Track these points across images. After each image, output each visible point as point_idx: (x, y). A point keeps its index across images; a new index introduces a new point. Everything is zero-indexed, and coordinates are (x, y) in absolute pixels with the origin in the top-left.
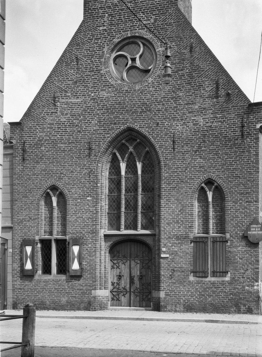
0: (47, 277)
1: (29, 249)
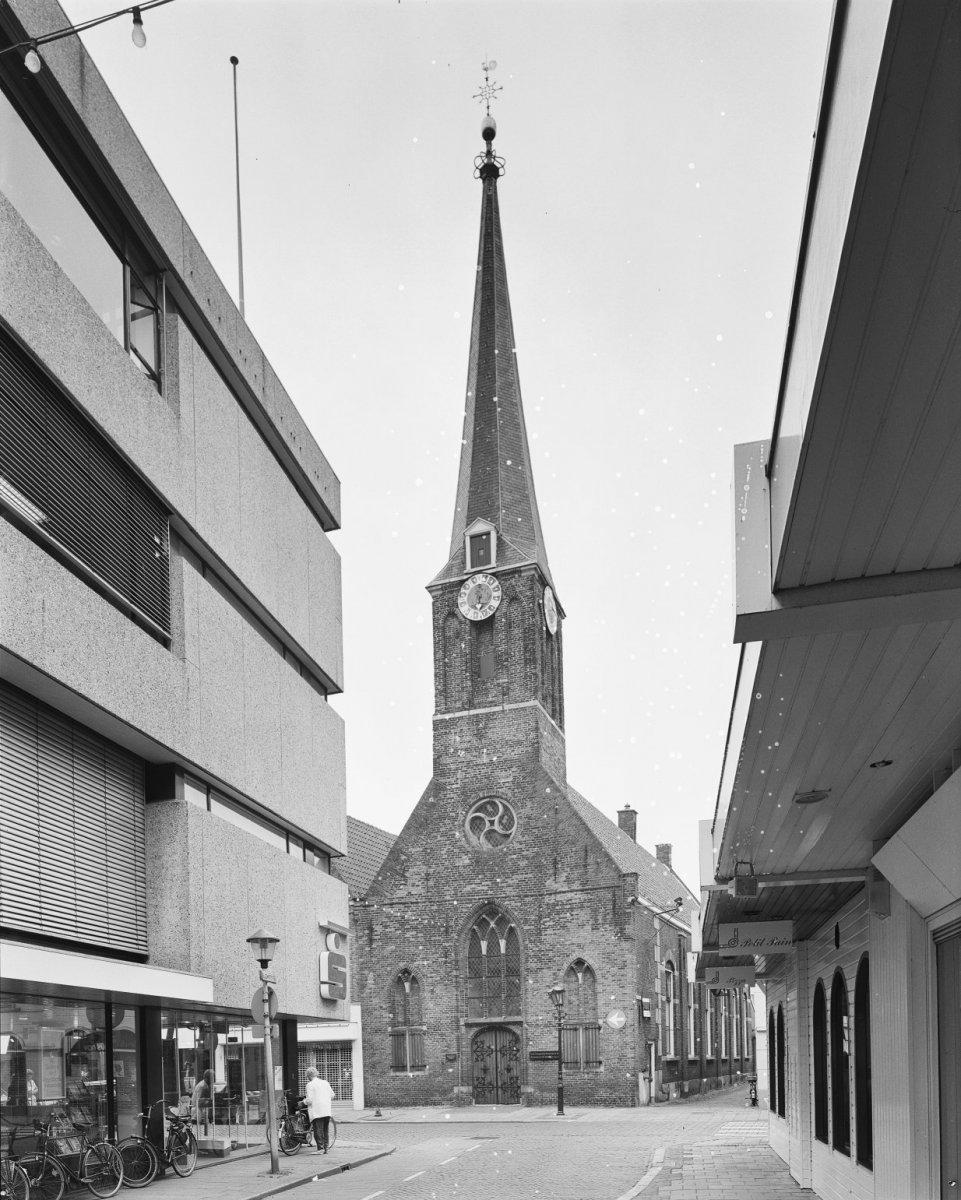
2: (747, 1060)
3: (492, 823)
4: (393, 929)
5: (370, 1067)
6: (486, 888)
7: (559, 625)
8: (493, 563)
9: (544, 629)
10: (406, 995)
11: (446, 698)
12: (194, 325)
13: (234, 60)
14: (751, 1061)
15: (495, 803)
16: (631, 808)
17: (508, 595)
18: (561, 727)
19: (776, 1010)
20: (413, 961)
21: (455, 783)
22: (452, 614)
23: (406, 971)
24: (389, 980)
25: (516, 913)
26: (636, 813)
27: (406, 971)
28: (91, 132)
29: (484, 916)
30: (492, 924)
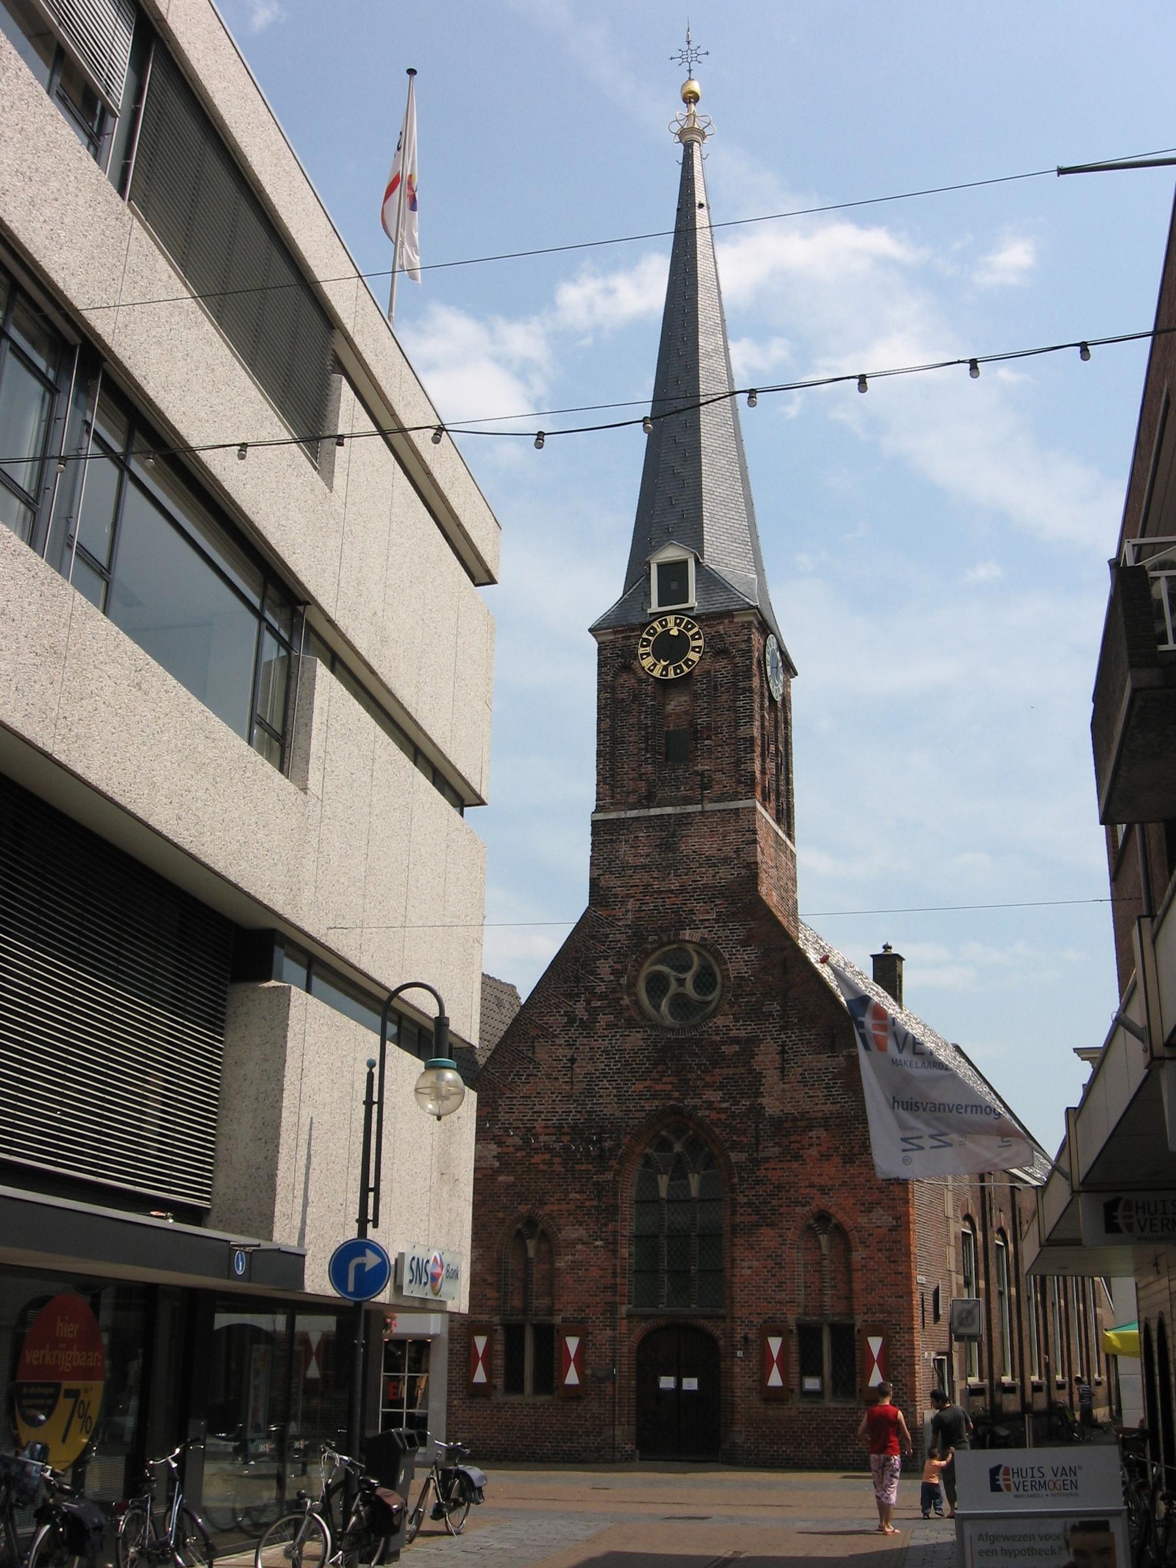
0: (515, 1399)
1: (480, 1342)
2: (1099, 1383)
3: (681, 982)
4: (512, 1149)
5: (465, 1391)
6: (669, 1087)
7: (786, 685)
8: (693, 601)
9: (767, 694)
10: (527, 1261)
11: (612, 787)
12: (412, 472)
13: (412, 72)
14: (1105, 1384)
15: (686, 951)
16: (893, 951)
17: (711, 647)
18: (790, 836)
19: (1154, 1325)
20: (542, 1203)
21: (627, 913)
22: (627, 668)
23: (531, 1222)
25: (717, 1131)
26: (902, 959)
27: (531, 1222)
28: (172, 26)
29: (663, 1133)
30: (678, 1148)
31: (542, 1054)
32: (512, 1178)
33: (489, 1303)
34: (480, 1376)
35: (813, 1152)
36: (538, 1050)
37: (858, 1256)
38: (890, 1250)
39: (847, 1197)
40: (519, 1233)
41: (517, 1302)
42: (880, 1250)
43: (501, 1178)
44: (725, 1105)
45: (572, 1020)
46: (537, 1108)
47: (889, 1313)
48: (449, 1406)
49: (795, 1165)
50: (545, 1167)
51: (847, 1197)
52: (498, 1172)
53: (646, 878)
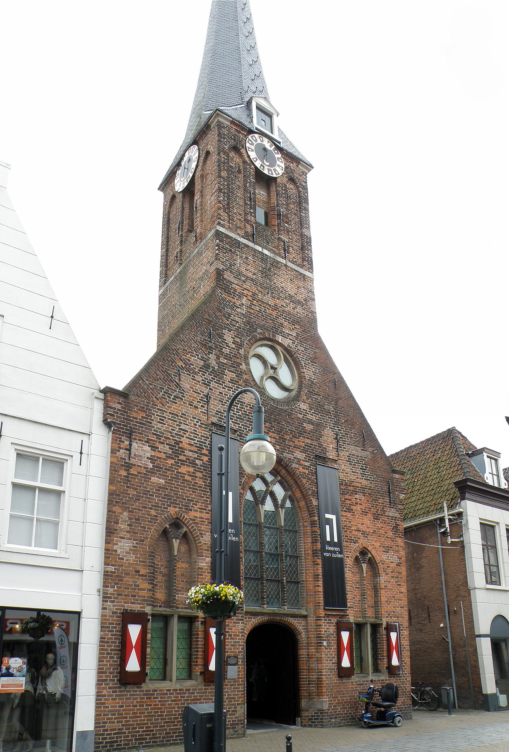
0: (165, 685)
1: (134, 631)
4: (164, 456)
20: (188, 510)
23: (176, 524)
24: (153, 531)
27: (176, 524)
31: (186, 382)
32: (162, 481)
33: (141, 593)
34: (133, 665)
35: (358, 508)
36: (183, 377)
37: (383, 579)
38: (397, 577)
39: (376, 541)
40: (165, 532)
41: (161, 595)
42: (392, 577)
43: (154, 479)
44: (307, 464)
45: (207, 366)
46: (183, 427)
47: (398, 617)
48: (99, 695)
49: (349, 515)
50: (189, 478)
51: (376, 541)
52: (152, 472)
53: (254, 289)
